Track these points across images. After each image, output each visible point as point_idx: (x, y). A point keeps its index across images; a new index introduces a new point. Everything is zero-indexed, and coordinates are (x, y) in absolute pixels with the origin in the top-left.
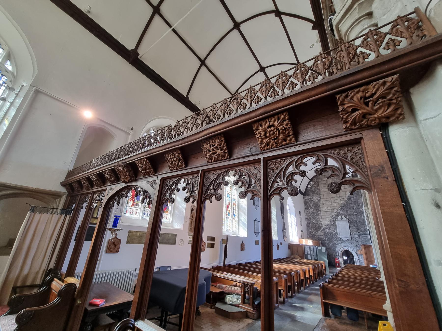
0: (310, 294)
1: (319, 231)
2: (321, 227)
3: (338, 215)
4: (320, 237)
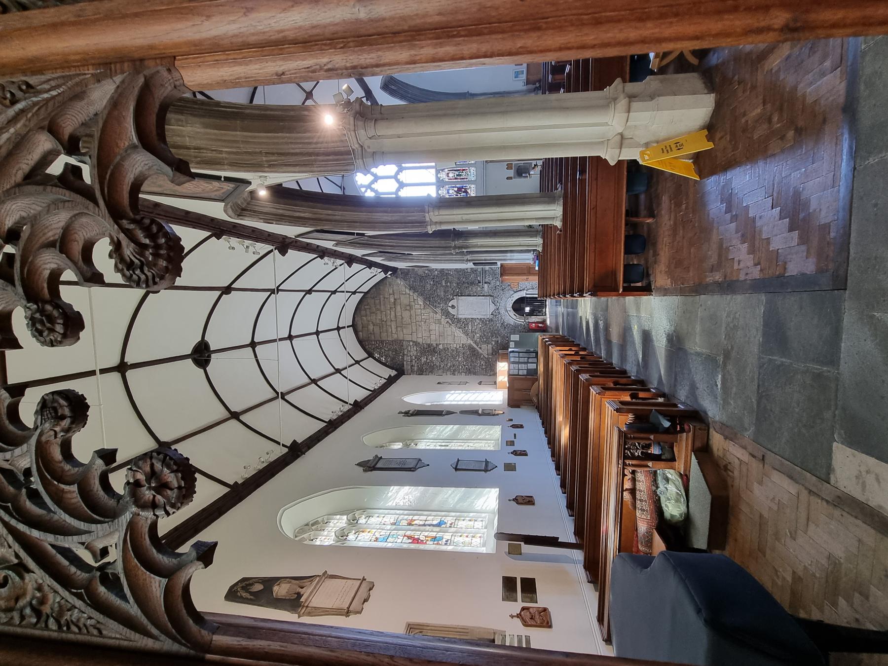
0: (609, 342)
1: (478, 352)
2: (471, 348)
3: (447, 314)
4: (490, 351)
